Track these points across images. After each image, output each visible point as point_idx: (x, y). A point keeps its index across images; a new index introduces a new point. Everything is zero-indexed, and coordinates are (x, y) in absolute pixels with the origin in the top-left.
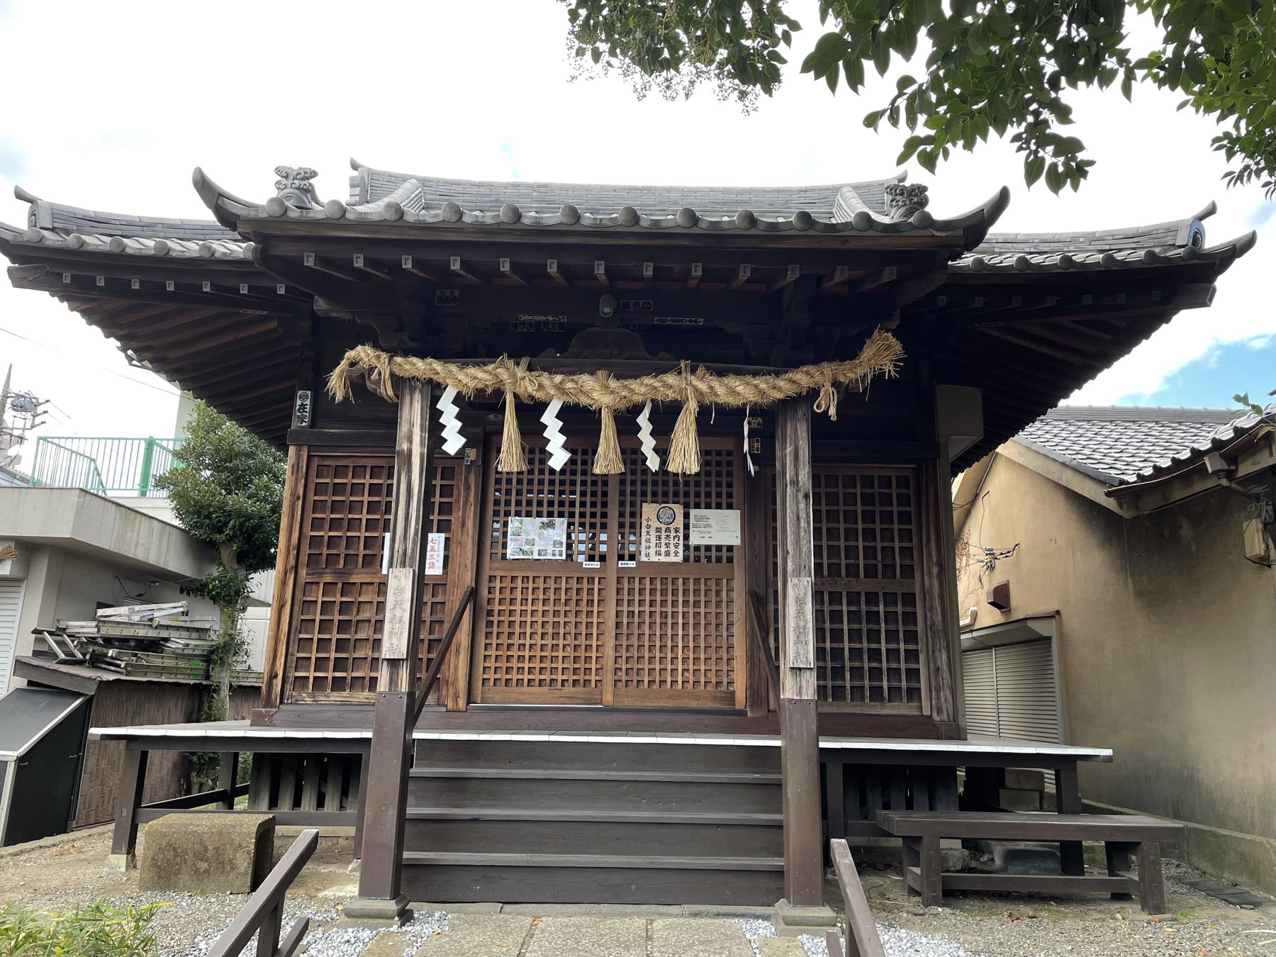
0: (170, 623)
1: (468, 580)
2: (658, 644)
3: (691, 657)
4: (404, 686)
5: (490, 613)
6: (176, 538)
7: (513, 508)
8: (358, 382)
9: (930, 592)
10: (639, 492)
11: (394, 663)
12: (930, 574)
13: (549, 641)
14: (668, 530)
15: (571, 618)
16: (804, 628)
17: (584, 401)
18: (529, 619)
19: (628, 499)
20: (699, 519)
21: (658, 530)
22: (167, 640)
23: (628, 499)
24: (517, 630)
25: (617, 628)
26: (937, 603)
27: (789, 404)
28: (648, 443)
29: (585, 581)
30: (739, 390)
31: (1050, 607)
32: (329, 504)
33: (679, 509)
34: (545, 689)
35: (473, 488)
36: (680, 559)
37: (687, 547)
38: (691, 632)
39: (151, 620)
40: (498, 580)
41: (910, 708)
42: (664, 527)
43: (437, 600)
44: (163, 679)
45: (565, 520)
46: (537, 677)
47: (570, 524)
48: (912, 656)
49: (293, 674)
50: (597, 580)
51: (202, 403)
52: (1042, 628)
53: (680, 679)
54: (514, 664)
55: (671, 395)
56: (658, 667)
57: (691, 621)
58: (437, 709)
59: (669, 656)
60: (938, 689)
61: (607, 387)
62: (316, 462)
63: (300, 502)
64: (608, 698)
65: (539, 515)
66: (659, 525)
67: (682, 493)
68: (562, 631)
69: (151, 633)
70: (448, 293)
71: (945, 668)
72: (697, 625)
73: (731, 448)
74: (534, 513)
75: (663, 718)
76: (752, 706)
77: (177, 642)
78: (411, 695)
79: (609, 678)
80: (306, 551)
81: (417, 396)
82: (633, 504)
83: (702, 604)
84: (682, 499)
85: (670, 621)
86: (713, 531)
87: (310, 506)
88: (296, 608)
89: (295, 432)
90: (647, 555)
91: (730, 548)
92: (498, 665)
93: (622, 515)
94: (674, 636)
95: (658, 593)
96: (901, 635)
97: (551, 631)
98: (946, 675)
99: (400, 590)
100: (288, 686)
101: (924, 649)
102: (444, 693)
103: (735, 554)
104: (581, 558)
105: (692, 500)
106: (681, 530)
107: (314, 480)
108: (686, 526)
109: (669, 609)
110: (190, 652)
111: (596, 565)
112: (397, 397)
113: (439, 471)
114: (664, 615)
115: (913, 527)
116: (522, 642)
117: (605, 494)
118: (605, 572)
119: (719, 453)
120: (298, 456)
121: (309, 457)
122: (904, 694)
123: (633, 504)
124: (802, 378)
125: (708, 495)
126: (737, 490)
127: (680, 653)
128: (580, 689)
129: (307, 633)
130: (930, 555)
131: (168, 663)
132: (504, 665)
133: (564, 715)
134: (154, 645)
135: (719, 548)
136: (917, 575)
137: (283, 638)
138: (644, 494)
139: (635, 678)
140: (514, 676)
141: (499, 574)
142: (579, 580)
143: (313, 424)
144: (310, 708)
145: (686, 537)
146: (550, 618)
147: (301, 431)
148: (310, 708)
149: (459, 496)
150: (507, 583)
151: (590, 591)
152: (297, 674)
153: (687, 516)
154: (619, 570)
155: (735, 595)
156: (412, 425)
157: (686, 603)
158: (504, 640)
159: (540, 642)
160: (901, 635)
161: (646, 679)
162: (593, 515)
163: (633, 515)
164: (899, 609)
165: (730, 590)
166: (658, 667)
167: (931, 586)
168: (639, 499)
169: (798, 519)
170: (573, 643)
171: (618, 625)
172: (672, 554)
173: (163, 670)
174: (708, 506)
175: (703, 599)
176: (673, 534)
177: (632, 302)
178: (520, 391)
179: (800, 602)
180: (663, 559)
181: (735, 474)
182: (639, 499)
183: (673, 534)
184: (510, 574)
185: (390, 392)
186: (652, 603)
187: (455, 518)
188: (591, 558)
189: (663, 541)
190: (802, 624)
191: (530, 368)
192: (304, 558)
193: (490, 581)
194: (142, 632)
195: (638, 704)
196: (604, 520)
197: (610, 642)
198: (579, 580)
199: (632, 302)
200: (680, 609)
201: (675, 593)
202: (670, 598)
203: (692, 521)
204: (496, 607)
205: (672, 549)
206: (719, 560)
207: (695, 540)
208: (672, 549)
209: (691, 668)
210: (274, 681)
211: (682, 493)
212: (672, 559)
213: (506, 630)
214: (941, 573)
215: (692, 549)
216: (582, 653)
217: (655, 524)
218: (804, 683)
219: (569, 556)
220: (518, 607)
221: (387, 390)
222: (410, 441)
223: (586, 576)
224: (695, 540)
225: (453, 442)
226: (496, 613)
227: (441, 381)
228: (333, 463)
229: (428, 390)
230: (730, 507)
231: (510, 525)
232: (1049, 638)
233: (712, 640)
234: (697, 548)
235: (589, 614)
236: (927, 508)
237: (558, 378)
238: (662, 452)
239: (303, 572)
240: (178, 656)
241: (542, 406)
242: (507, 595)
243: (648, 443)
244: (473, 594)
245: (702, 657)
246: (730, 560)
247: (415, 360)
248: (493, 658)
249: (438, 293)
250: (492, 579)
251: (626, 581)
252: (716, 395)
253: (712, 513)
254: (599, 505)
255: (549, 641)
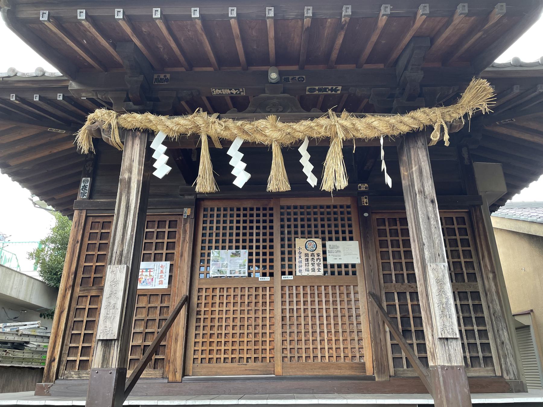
0: (29, 333)
1: (185, 291)
2: (311, 331)
3: (334, 339)
4: (114, 363)
5: (198, 313)
6: (37, 285)
7: (214, 245)
8: (97, 140)
9: (490, 290)
10: (293, 232)
11: (107, 343)
12: (488, 278)
13: (237, 331)
14: (313, 255)
15: (252, 315)
16: (447, 303)
17: (259, 139)
18: (224, 316)
19: (286, 236)
20: (332, 247)
21: (306, 255)
22: (28, 343)
23: (286, 236)
24: (217, 324)
25: (282, 320)
26: (495, 297)
27: (413, 136)
28: (308, 168)
29: (261, 289)
30: (375, 126)
31: (526, 309)
32: (97, 245)
33: (319, 242)
34: (235, 365)
35: (188, 232)
36: (321, 273)
37: (325, 266)
38: (332, 322)
39: (18, 331)
40: (204, 291)
41: (487, 371)
42: (310, 253)
43: (164, 305)
44: (23, 365)
45: (247, 251)
46: (230, 356)
47: (250, 254)
48: (483, 334)
49: (66, 358)
50: (268, 289)
51: (59, 214)
52: (525, 321)
53: (327, 355)
54: (215, 347)
55: (323, 133)
56: (311, 347)
57: (332, 315)
58: (162, 381)
59: (319, 339)
60: (505, 356)
61: (276, 127)
62: (91, 220)
63: (79, 244)
64: (279, 370)
65: (230, 248)
66: (307, 252)
67: (320, 232)
68: (246, 324)
69: (17, 339)
70: (162, 76)
71: (507, 341)
72: (336, 316)
73: (349, 203)
74: (227, 247)
75: (318, 383)
76: (378, 373)
77: (34, 344)
78: (121, 373)
79: (278, 356)
80: (80, 275)
81: (137, 141)
82: (289, 240)
83: (338, 302)
84: (320, 235)
85: (317, 315)
86: (342, 254)
87: (85, 247)
88: (71, 313)
89: (79, 202)
90: (300, 271)
91: (354, 266)
92: (204, 348)
93: (282, 246)
94: (321, 324)
95: (309, 296)
96: (474, 320)
97: (239, 324)
98: (508, 346)
99: (115, 283)
100: (62, 367)
101: (491, 330)
102: (167, 369)
103: (357, 269)
104: (258, 275)
105: (327, 235)
106: (321, 255)
107: (88, 230)
108: (324, 252)
109: (317, 307)
110: (41, 350)
111: (268, 279)
112: (123, 143)
113: (168, 223)
114: (313, 310)
115: (471, 248)
116: (219, 332)
117: (271, 234)
118: (273, 283)
119: (341, 207)
120: (80, 216)
121: (87, 217)
122: (482, 361)
123: (289, 240)
124: (420, 117)
125: (337, 232)
126: (355, 229)
127: (326, 337)
128: (259, 363)
129: (77, 330)
130: (486, 266)
131: (26, 356)
132: (208, 348)
133: (249, 384)
134: (19, 346)
135: (346, 266)
136: (479, 279)
137: (61, 334)
138: (296, 233)
139: (296, 355)
140: (215, 356)
141: (204, 287)
142: (257, 289)
143: (90, 197)
144: (76, 382)
145: (325, 259)
146: (238, 315)
147: (82, 202)
148: (76, 382)
149: (179, 238)
150: (210, 293)
151: (264, 296)
152: (69, 359)
153: (324, 246)
154: (283, 281)
155: (359, 296)
156: (132, 161)
157: (327, 302)
158: (208, 331)
159: (231, 332)
160: (474, 320)
161: (304, 356)
162: (264, 247)
163: (290, 246)
164: (470, 302)
165: (356, 293)
166: (311, 347)
167: (490, 286)
168: (293, 236)
169: (429, 218)
170: (254, 331)
171: (283, 318)
172: (316, 270)
173: (24, 360)
174: (337, 239)
175: (338, 299)
176: (316, 257)
177: (290, 77)
178: (212, 133)
179: (440, 283)
180: (311, 273)
181: (353, 219)
182: (293, 236)
183: (316, 257)
184: (212, 287)
185: (118, 140)
186: (305, 302)
187: (177, 251)
188: (264, 275)
189: (310, 262)
190: (444, 300)
191: (219, 118)
192: (79, 280)
193: (199, 292)
194: (11, 338)
195: (299, 374)
196: (271, 250)
197: (278, 330)
198: (257, 289)
199: (290, 77)
200: (324, 307)
201: (319, 295)
202: (317, 299)
203: (328, 249)
204: (203, 309)
205: (316, 267)
206: (347, 273)
207: (330, 261)
208: (316, 267)
209: (334, 347)
210: (53, 364)
211: (320, 232)
212: (317, 273)
213: (209, 324)
214: (495, 277)
215: (329, 266)
216: (260, 339)
217: (304, 251)
218: (452, 351)
219: (249, 275)
220: (217, 308)
221: (115, 138)
222: (130, 171)
223: (261, 286)
224: (330, 261)
225: (162, 169)
226: (202, 313)
227: (153, 128)
228: (101, 220)
229: (145, 138)
230: (351, 239)
231: (212, 255)
232: (528, 326)
233: (347, 327)
234: (332, 266)
235: (264, 311)
236: (479, 236)
237: (239, 123)
238: (318, 171)
239: (78, 289)
240: (34, 352)
241: (227, 143)
242: (210, 301)
243: (308, 168)
244: (187, 300)
245: (341, 339)
246: (354, 273)
247: (135, 115)
248: (201, 344)
249: (155, 76)
250: (200, 290)
251: (287, 288)
252: (357, 130)
253: (340, 244)
254: (268, 241)
255: (237, 331)
